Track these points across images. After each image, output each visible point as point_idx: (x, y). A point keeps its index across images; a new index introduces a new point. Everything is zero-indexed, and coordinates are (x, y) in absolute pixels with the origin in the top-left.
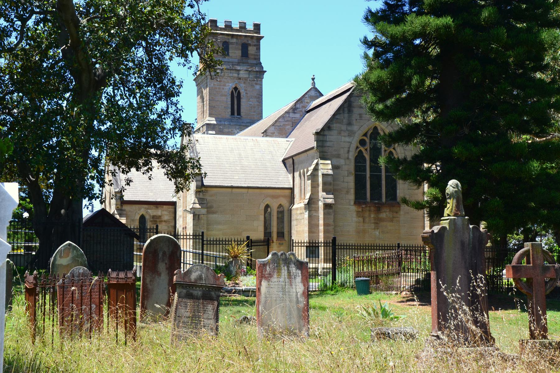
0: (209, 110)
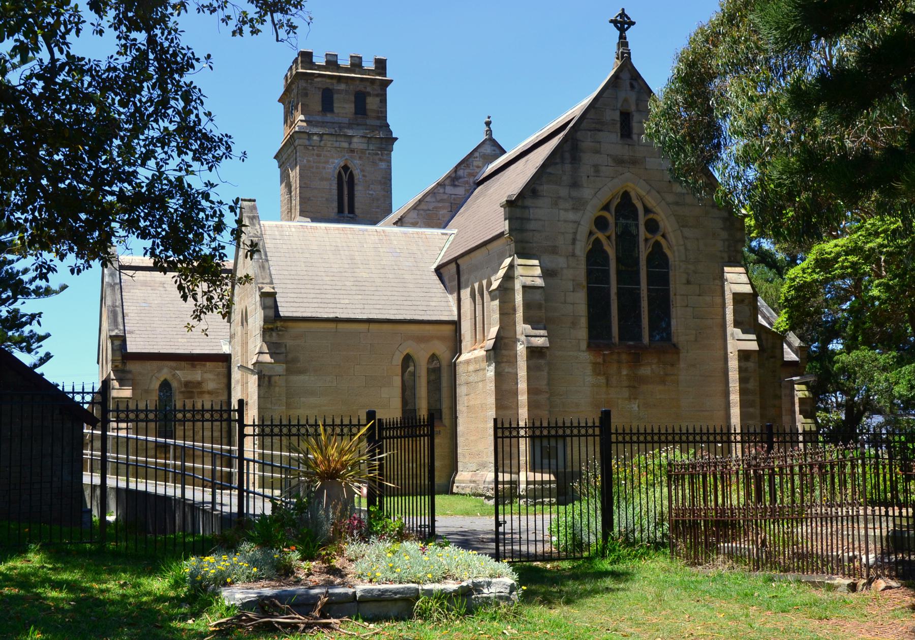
0: (300, 204)
